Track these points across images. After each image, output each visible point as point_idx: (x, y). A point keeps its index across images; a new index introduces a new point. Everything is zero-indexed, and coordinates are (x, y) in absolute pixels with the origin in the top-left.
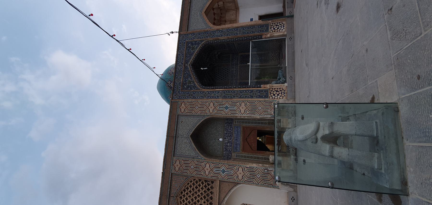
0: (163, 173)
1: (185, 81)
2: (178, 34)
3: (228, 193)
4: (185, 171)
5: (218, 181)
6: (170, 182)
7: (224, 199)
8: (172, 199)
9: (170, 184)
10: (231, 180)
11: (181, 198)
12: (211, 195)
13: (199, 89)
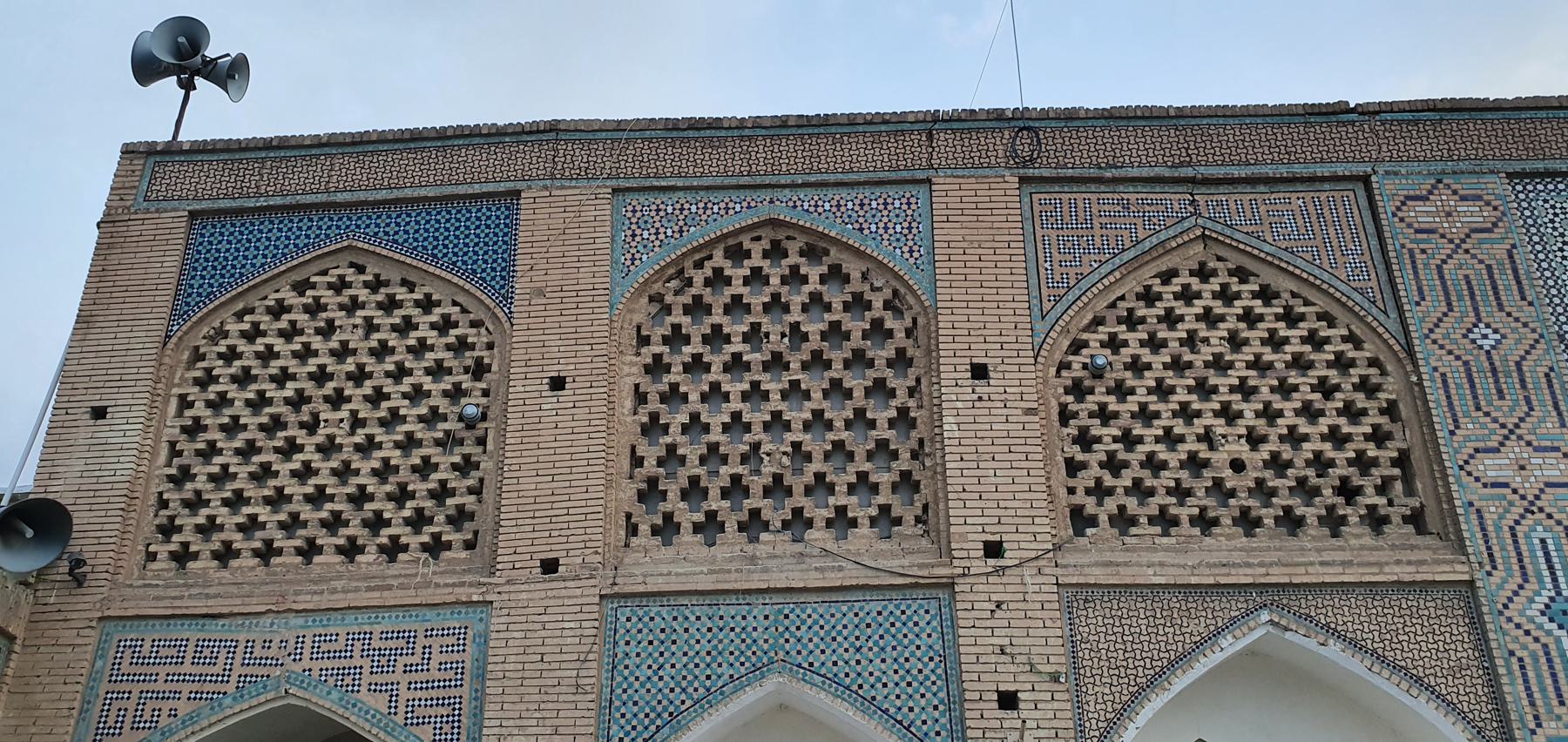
2: (163, 135)
4: (1429, 278)
5: (1460, 573)
6: (1299, 170)
7: (1331, 631)
8: (1176, 199)
9: (1283, 171)
10: (1513, 690)
11: (1203, 273)
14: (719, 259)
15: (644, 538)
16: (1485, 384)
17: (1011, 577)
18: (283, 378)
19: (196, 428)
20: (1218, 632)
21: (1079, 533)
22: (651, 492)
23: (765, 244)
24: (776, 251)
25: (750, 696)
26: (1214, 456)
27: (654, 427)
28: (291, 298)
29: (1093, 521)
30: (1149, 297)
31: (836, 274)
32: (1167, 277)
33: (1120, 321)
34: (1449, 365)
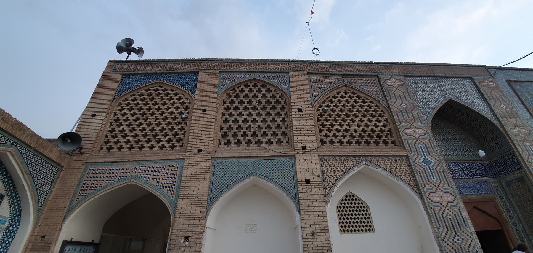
0: (371, 63)
3: (393, 174)
4: (392, 94)
7: (379, 166)
8: (339, 78)
11: (346, 93)
12: (264, 140)
14: (242, 86)
16: (405, 115)
17: (308, 154)
20: (354, 166)
21: (322, 145)
22: (225, 135)
23: (253, 84)
24: (255, 85)
25: (247, 181)
26: (351, 129)
27: (226, 121)
29: (325, 142)
30: (335, 97)
31: (268, 90)
33: (329, 101)
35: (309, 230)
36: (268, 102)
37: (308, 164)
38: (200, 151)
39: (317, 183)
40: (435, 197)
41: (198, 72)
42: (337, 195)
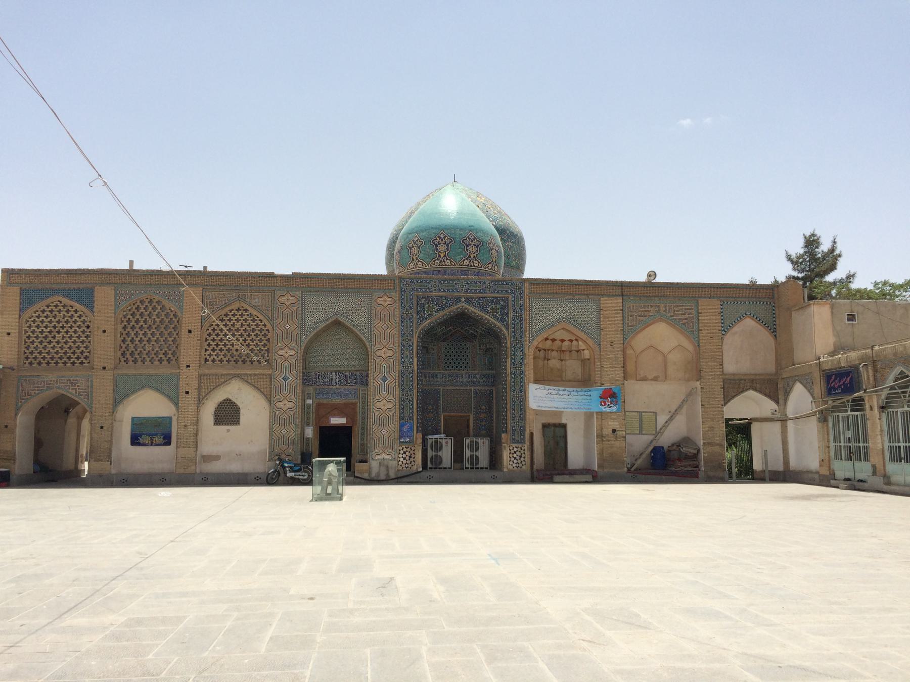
1: (433, 300)
10: (273, 391)
13: (417, 328)
15: (123, 363)
18: (46, 327)
19: (29, 337)
22: (123, 354)
27: (124, 341)
28: (46, 309)
32: (48, 306)
34: (280, 333)
35: (183, 424)
36: (162, 322)
37: (189, 378)
38: (104, 368)
39: (194, 393)
40: (280, 405)
41: (699, 378)
42: (219, 396)
